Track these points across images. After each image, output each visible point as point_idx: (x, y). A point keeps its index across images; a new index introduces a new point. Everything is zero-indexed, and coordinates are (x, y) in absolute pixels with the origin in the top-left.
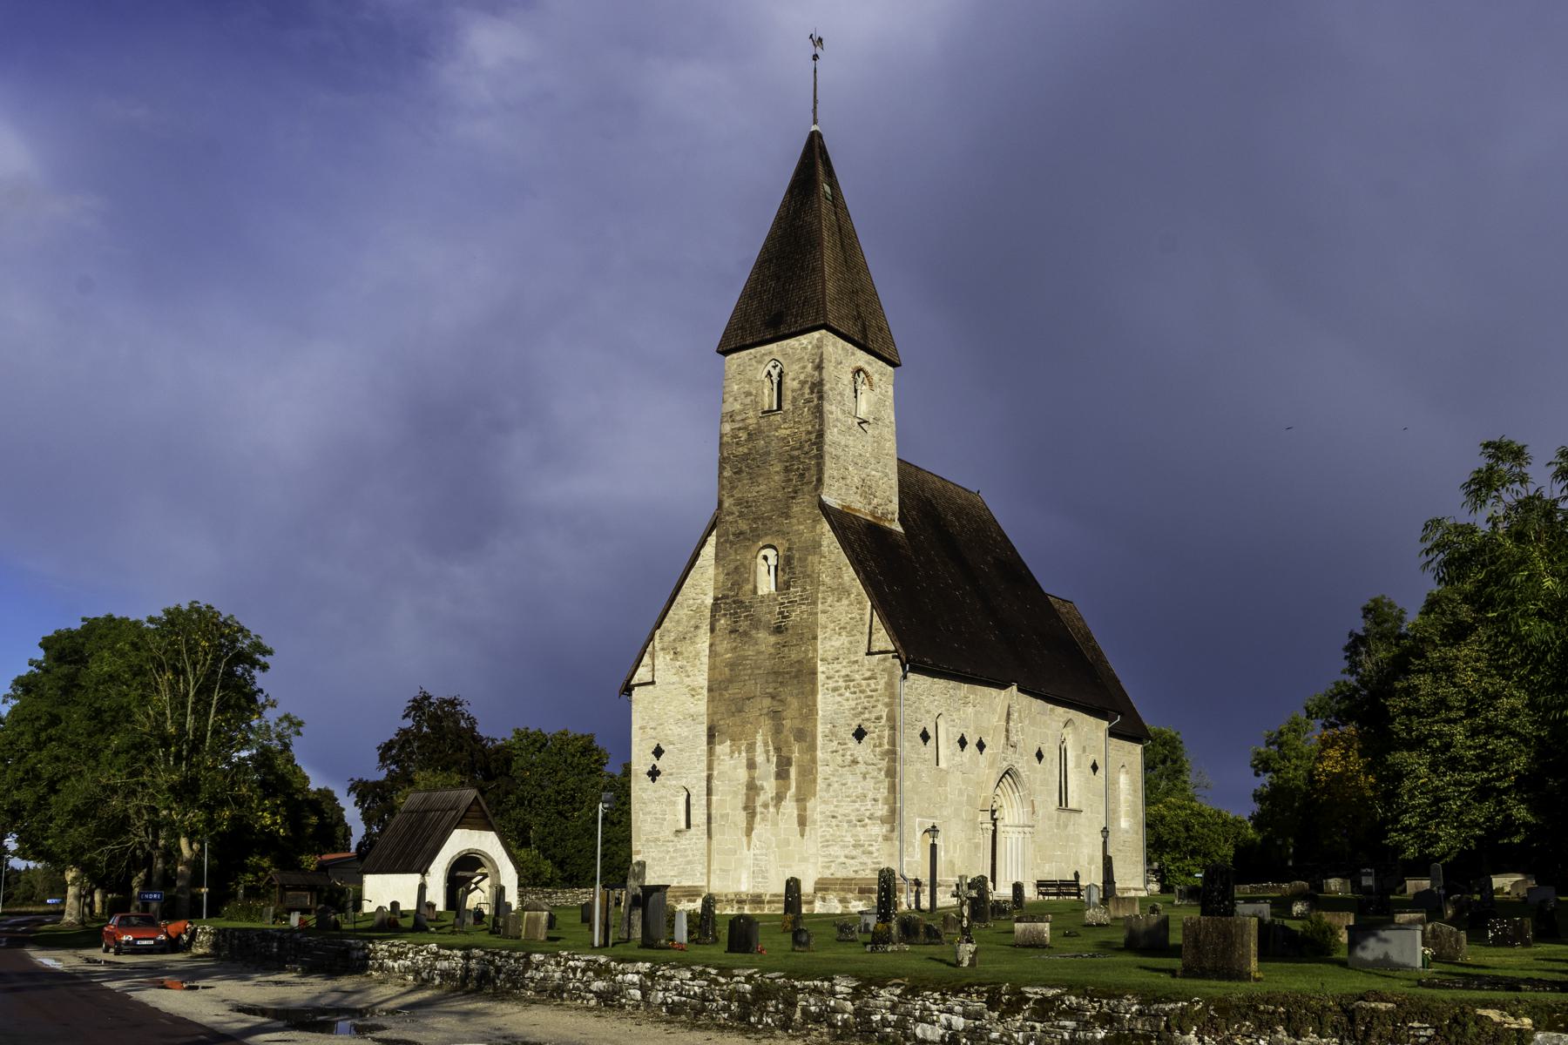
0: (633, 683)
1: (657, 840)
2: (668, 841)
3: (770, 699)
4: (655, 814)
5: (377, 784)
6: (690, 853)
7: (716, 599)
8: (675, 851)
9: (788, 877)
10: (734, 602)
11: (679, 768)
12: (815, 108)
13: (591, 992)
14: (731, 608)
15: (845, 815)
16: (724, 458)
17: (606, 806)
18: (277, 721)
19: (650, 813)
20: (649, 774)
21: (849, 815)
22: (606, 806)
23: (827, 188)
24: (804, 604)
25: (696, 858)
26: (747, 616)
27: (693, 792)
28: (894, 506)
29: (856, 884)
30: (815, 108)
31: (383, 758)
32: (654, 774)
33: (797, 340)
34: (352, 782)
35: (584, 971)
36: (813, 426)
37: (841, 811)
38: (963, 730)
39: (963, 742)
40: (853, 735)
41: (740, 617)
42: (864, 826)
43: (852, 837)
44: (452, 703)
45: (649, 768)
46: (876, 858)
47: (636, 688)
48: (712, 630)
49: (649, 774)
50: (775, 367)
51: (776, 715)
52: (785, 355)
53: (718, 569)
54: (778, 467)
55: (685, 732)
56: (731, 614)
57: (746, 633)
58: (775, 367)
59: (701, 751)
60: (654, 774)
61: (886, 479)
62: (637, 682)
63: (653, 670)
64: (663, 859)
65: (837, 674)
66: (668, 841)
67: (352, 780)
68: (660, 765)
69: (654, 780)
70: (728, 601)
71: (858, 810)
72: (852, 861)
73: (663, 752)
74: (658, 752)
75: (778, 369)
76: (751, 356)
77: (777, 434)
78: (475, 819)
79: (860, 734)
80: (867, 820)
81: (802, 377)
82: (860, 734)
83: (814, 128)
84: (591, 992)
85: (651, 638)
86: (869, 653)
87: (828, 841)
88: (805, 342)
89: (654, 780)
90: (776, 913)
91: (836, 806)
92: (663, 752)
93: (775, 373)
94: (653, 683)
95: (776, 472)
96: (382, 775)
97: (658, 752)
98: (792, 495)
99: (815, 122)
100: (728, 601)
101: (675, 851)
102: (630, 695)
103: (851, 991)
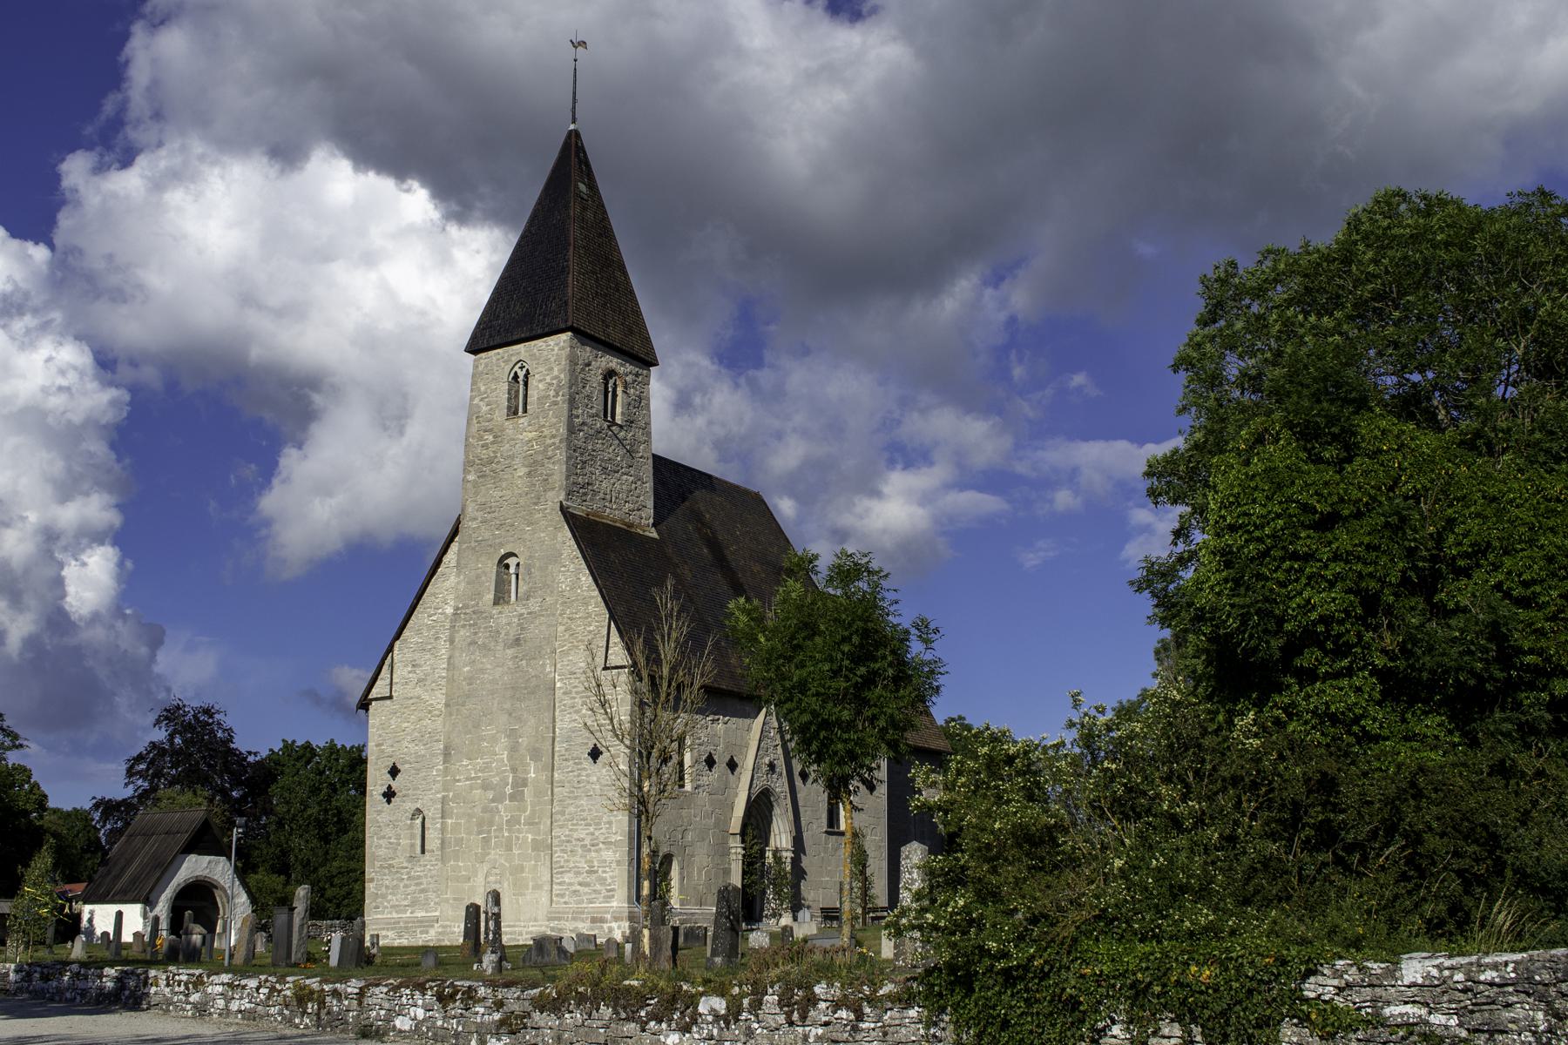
0: (370, 697)
1: (391, 866)
2: (403, 868)
3: (507, 716)
4: (390, 838)
5: (119, 804)
6: (424, 880)
7: (457, 609)
8: (409, 878)
9: (468, 903)
10: (474, 612)
11: (414, 789)
12: (574, 108)
13: (190, 1003)
14: (471, 619)
15: (578, 840)
16: (468, 462)
17: (240, 830)
18: (1260, 257)
19: (384, 837)
20: (385, 795)
21: (583, 840)
22: (240, 830)
23: (582, 187)
24: (543, 616)
25: (431, 886)
26: (486, 628)
27: (429, 814)
28: (649, 512)
29: (588, 913)
30: (574, 108)
31: (130, 773)
32: (389, 795)
33: (545, 342)
34: (94, 801)
35: (186, 984)
36: (558, 430)
37: (575, 835)
38: (710, 748)
39: (710, 762)
40: (589, 754)
41: (479, 628)
42: (596, 851)
43: (586, 862)
44: (208, 712)
45: (385, 789)
46: (609, 885)
47: (373, 703)
48: (452, 641)
49: (385, 795)
50: (522, 368)
51: (512, 734)
52: (532, 356)
53: (459, 577)
54: (522, 471)
55: (421, 750)
56: (470, 625)
57: (484, 647)
58: (522, 368)
59: (437, 770)
60: (389, 795)
61: (639, 483)
62: (375, 696)
63: (391, 684)
64: (396, 887)
65: (574, 690)
66: (403, 868)
67: (94, 798)
68: (395, 785)
69: (389, 802)
70: (468, 611)
71: (593, 834)
72: (586, 889)
73: (399, 771)
74: (394, 772)
75: (524, 370)
76: (499, 357)
77: (521, 437)
78: (204, 841)
79: (595, 754)
80: (601, 845)
81: (548, 379)
82: (595, 754)
83: (572, 127)
84: (190, 1003)
85: (390, 649)
86: (605, 668)
87: (562, 867)
88: (552, 343)
89: (389, 802)
90: (220, 922)
91: (571, 830)
92: (399, 771)
93: (521, 374)
94: (390, 697)
95: (519, 477)
96: (129, 792)
97: (394, 772)
98: (535, 500)
99: (574, 122)
100: (468, 611)
101: (409, 878)
102: (367, 710)
103: (358, 991)
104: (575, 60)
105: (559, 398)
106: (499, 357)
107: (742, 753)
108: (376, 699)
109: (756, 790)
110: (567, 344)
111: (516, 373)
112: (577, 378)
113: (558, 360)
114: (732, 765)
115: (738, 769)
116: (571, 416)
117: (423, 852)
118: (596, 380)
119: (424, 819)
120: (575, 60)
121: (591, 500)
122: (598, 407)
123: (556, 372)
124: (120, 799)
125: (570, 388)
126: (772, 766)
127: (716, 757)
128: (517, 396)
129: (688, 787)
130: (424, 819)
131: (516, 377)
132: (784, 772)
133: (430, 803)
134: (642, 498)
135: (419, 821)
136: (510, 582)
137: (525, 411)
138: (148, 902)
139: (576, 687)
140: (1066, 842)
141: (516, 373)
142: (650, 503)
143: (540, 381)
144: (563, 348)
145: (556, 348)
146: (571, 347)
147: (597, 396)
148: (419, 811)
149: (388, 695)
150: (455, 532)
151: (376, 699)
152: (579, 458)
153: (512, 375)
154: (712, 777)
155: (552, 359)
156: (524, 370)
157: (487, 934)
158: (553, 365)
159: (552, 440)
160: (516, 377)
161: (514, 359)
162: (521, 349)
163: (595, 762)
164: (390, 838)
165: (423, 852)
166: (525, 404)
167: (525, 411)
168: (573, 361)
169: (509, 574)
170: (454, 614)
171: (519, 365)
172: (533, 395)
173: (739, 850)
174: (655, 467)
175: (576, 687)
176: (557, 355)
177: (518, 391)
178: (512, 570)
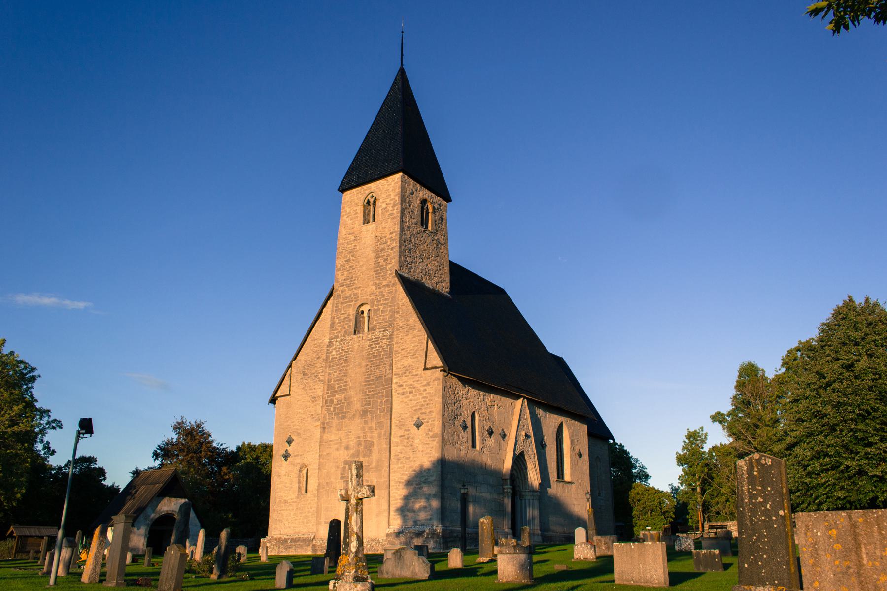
32: (286, 456)
39: (491, 433)
47: (279, 399)
68: (290, 449)
69: (286, 460)
75: (374, 198)
76: (358, 192)
85: (290, 366)
86: (425, 369)
89: (286, 460)
93: (372, 201)
94: (289, 395)
104: (402, 32)
105: (395, 211)
106: (358, 192)
107: (508, 428)
108: (281, 397)
109: (518, 452)
110: (400, 180)
111: (368, 201)
112: (405, 200)
113: (394, 190)
114: (504, 436)
115: (507, 438)
116: (402, 222)
117: (306, 492)
118: (417, 204)
119: (308, 470)
120: (402, 32)
121: (414, 272)
122: (418, 218)
123: (392, 197)
124: (87, 456)
125: (402, 204)
126: (527, 436)
127: (493, 429)
128: (369, 214)
129: (478, 447)
130: (308, 470)
131: (368, 202)
132: (533, 441)
133: (311, 459)
134: (443, 276)
135: (304, 472)
136: (364, 322)
137: (374, 220)
138: (703, 554)
139: (405, 382)
140: (714, 479)
141: (368, 201)
142: (448, 279)
143: (383, 203)
144: (397, 183)
145: (393, 183)
146: (402, 182)
147: (417, 211)
148: (303, 466)
149: (288, 393)
150: (331, 295)
151: (281, 397)
152: (406, 247)
153: (366, 201)
154: (491, 441)
155: (390, 190)
156: (374, 198)
157: (140, 493)
158: (391, 193)
159: (391, 236)
160: (368, 202)
161: (367, 192)
162: (372, 186)
163: (419, 429)
164: (286, 483)
165: (306, 492)
166: (374, 215)
167: (374, 220)
168: (403, 189)
169: (363, 318)
170: (329, 342)
171: (370, 195)
172: (379, 211)
173: (509, 490)
174: (450, 264)
175: (405, 382)
176: (393, 187)
177: (369, 211)
178: (365, 314)
